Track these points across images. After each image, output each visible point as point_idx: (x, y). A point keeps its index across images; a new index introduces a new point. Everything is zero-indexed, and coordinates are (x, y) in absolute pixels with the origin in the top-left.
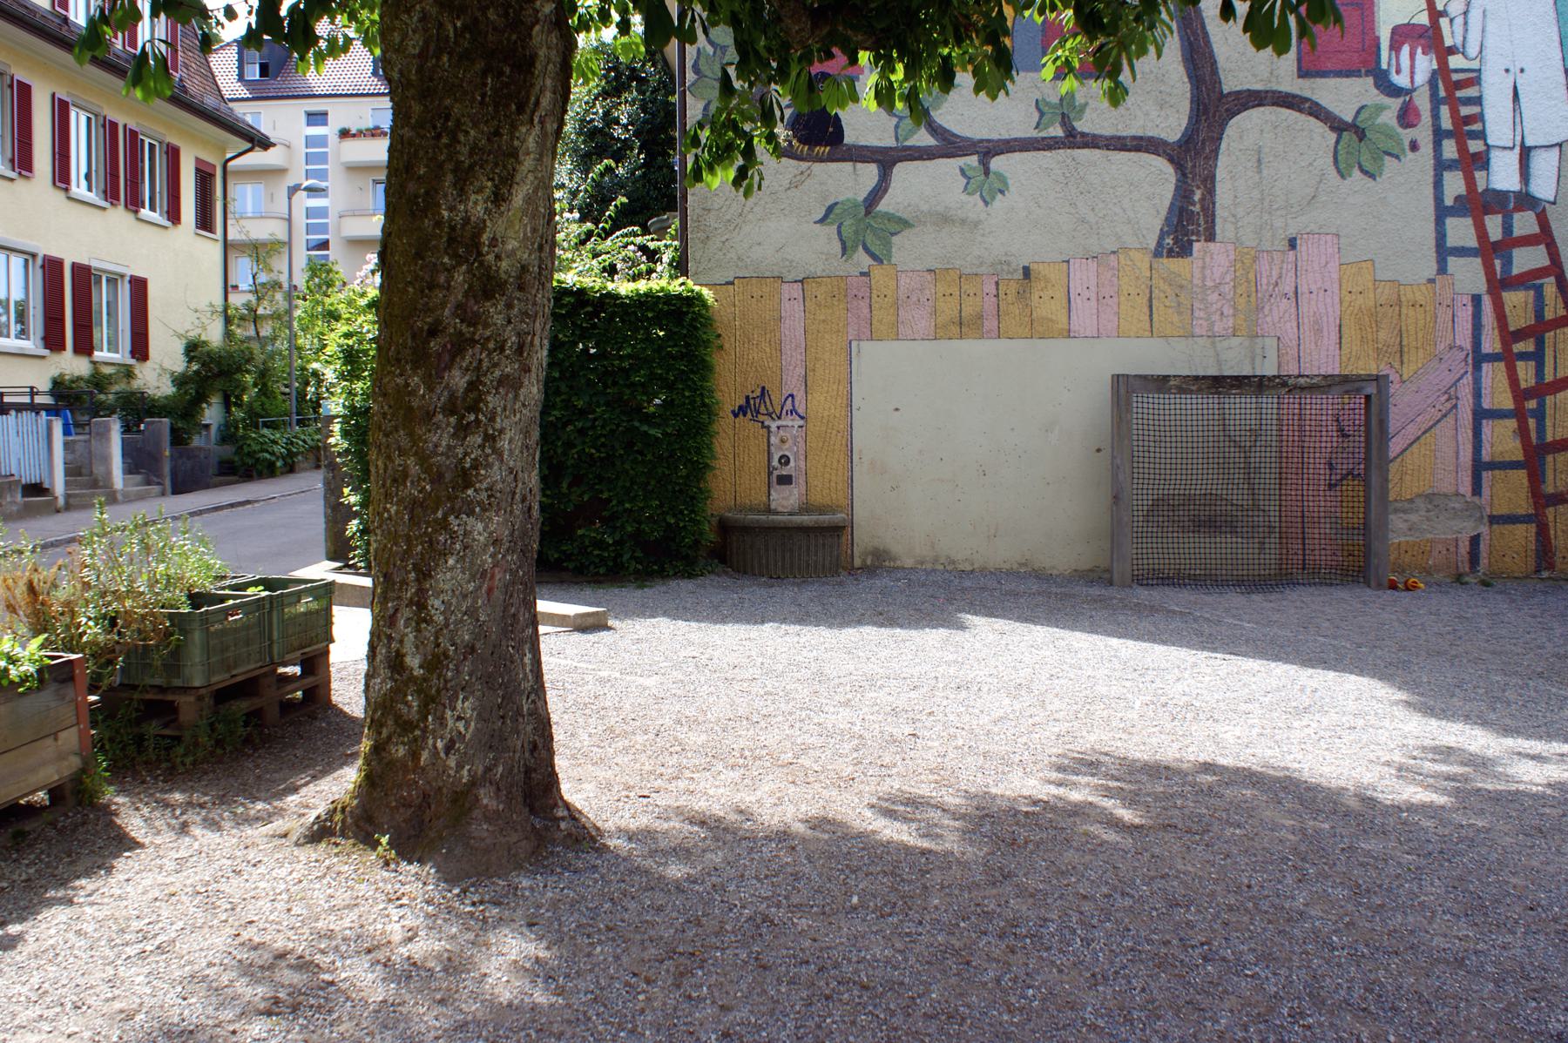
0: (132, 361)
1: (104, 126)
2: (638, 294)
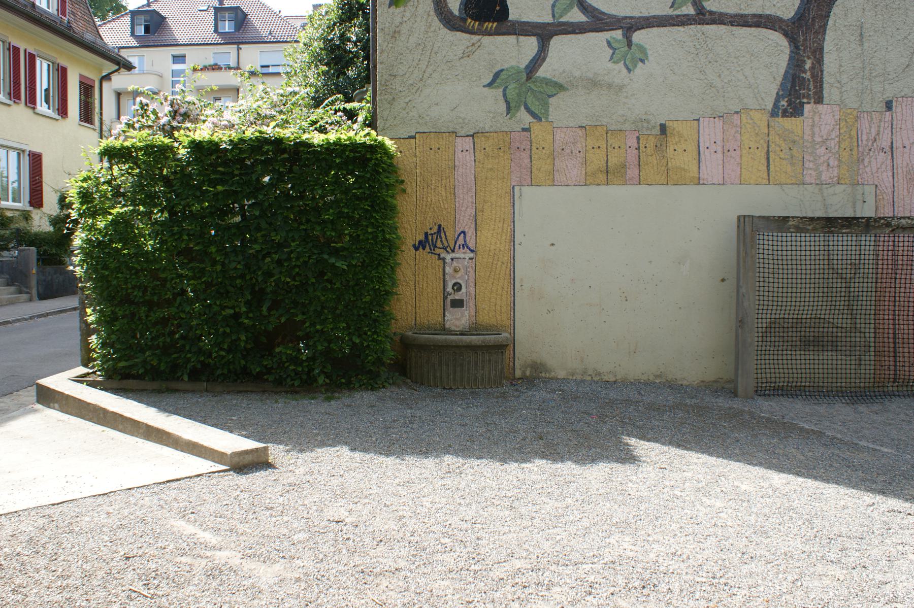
0: (31, 208)
1: (9, 49)
2: (328, 143)
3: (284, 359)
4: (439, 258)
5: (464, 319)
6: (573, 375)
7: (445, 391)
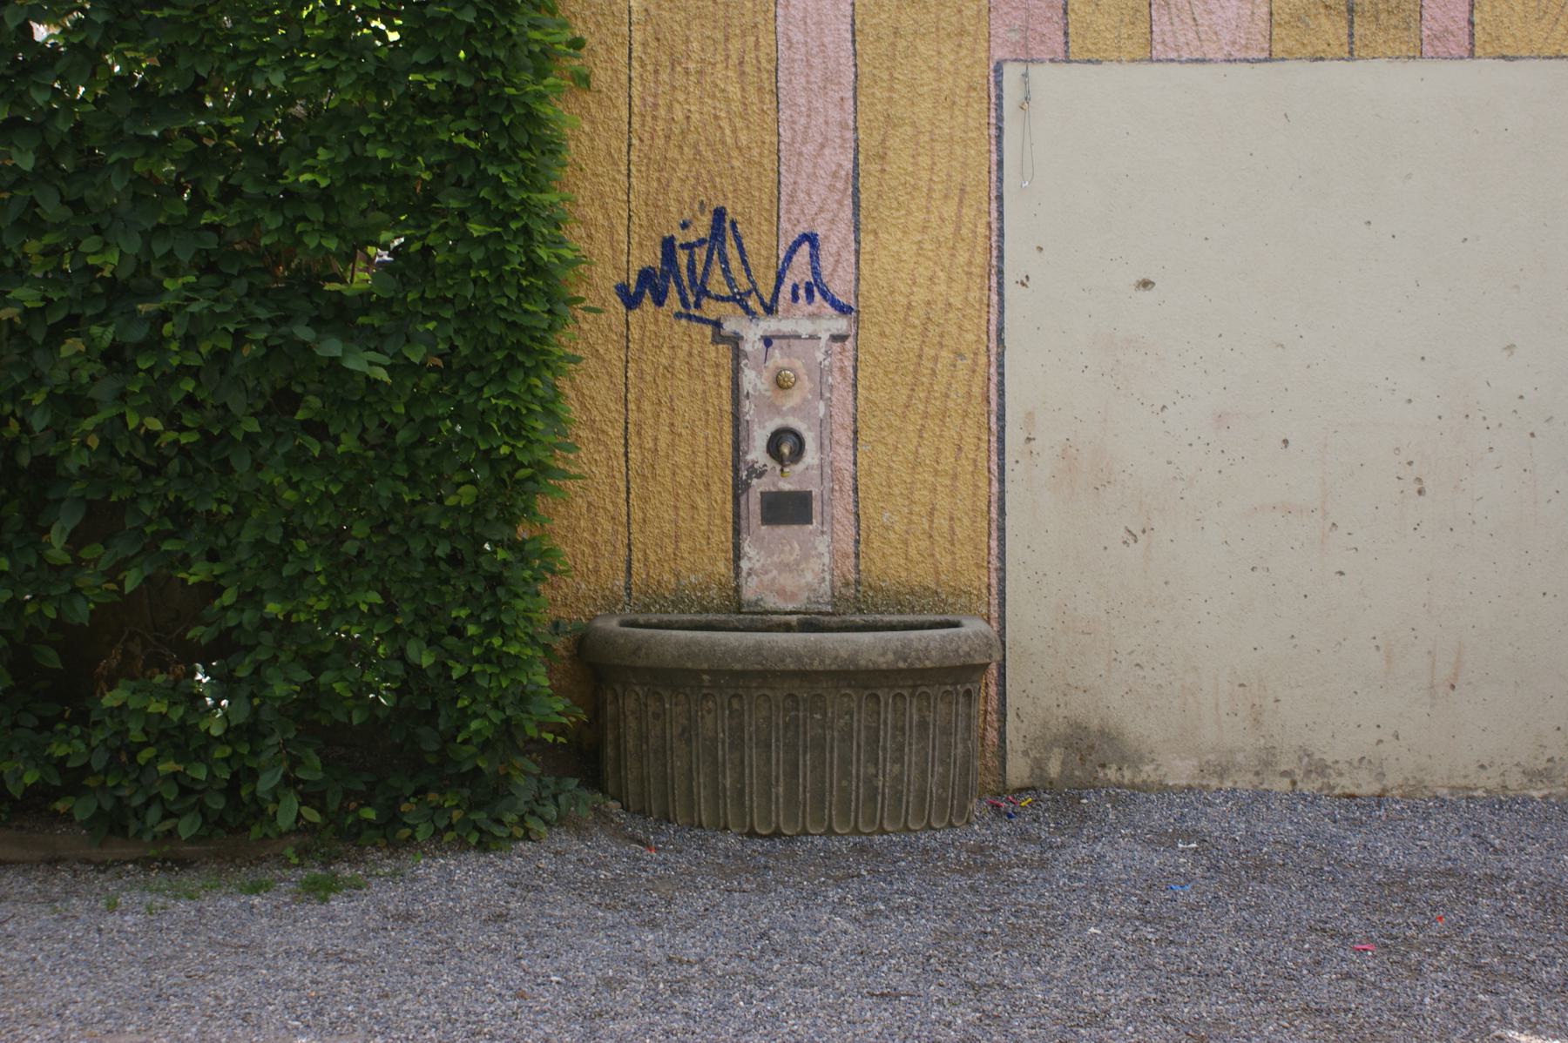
3: (136, 735)
4: (719, 338)
5: (815, 565)
6: (1222, 773)
7: (757, 845)
